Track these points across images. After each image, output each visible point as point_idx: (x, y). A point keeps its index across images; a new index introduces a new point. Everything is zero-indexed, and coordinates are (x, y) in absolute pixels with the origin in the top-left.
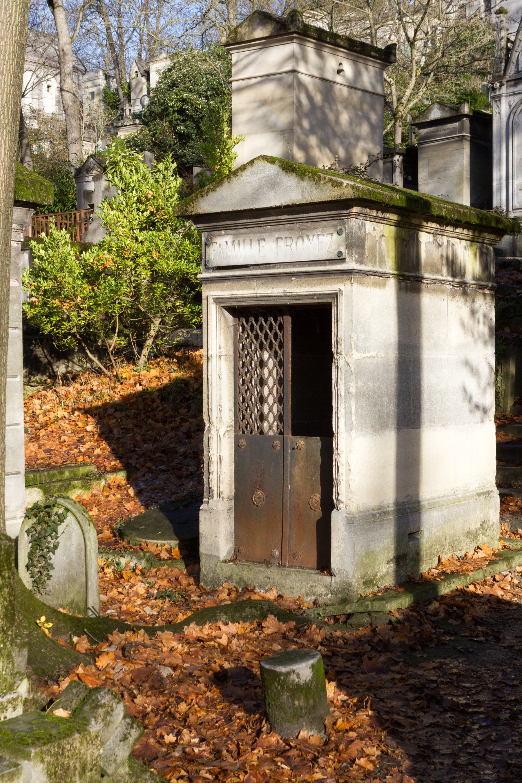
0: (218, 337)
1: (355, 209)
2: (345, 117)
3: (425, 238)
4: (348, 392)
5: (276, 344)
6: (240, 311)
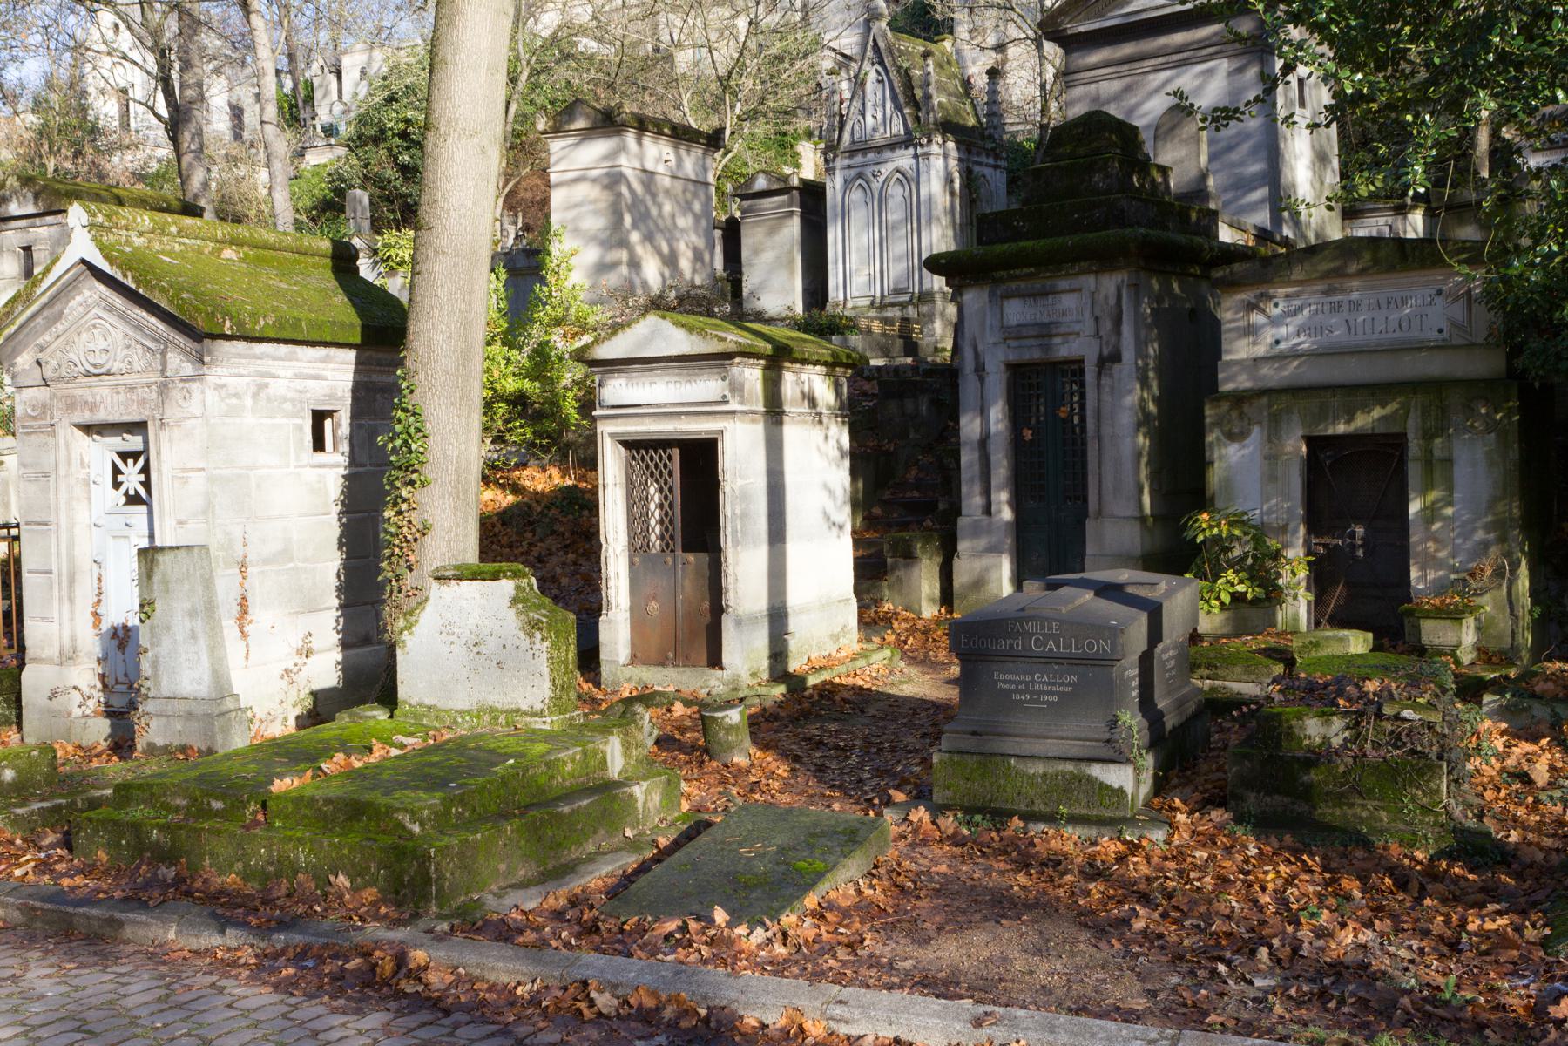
0: (612, 465)
1: (737, 360)
2: (668, 208)
3: (788, 378)
4: (734, 513)
5: (666, 473)
6: (633, 445)
